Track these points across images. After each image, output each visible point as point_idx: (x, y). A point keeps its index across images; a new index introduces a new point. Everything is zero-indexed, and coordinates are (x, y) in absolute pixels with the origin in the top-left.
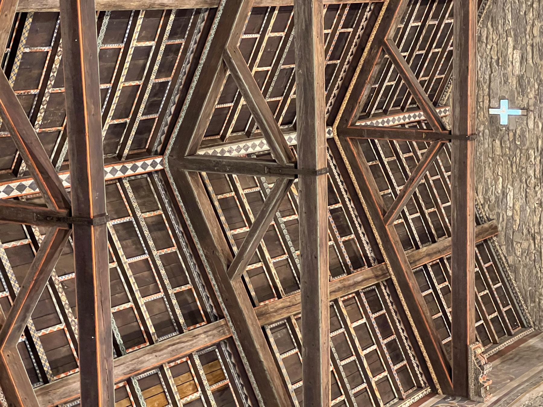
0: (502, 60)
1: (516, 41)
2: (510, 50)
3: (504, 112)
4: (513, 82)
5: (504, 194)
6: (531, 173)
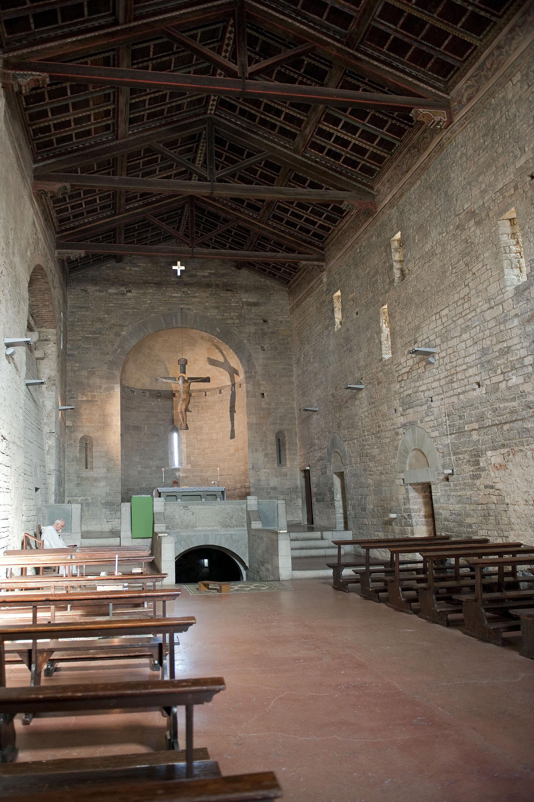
0: (202, 268)
1: (213, 274)
2: (209, 271)
3: (179, 268)
4: (193, 272)
5: (138, 266)
6: (149, 278)
